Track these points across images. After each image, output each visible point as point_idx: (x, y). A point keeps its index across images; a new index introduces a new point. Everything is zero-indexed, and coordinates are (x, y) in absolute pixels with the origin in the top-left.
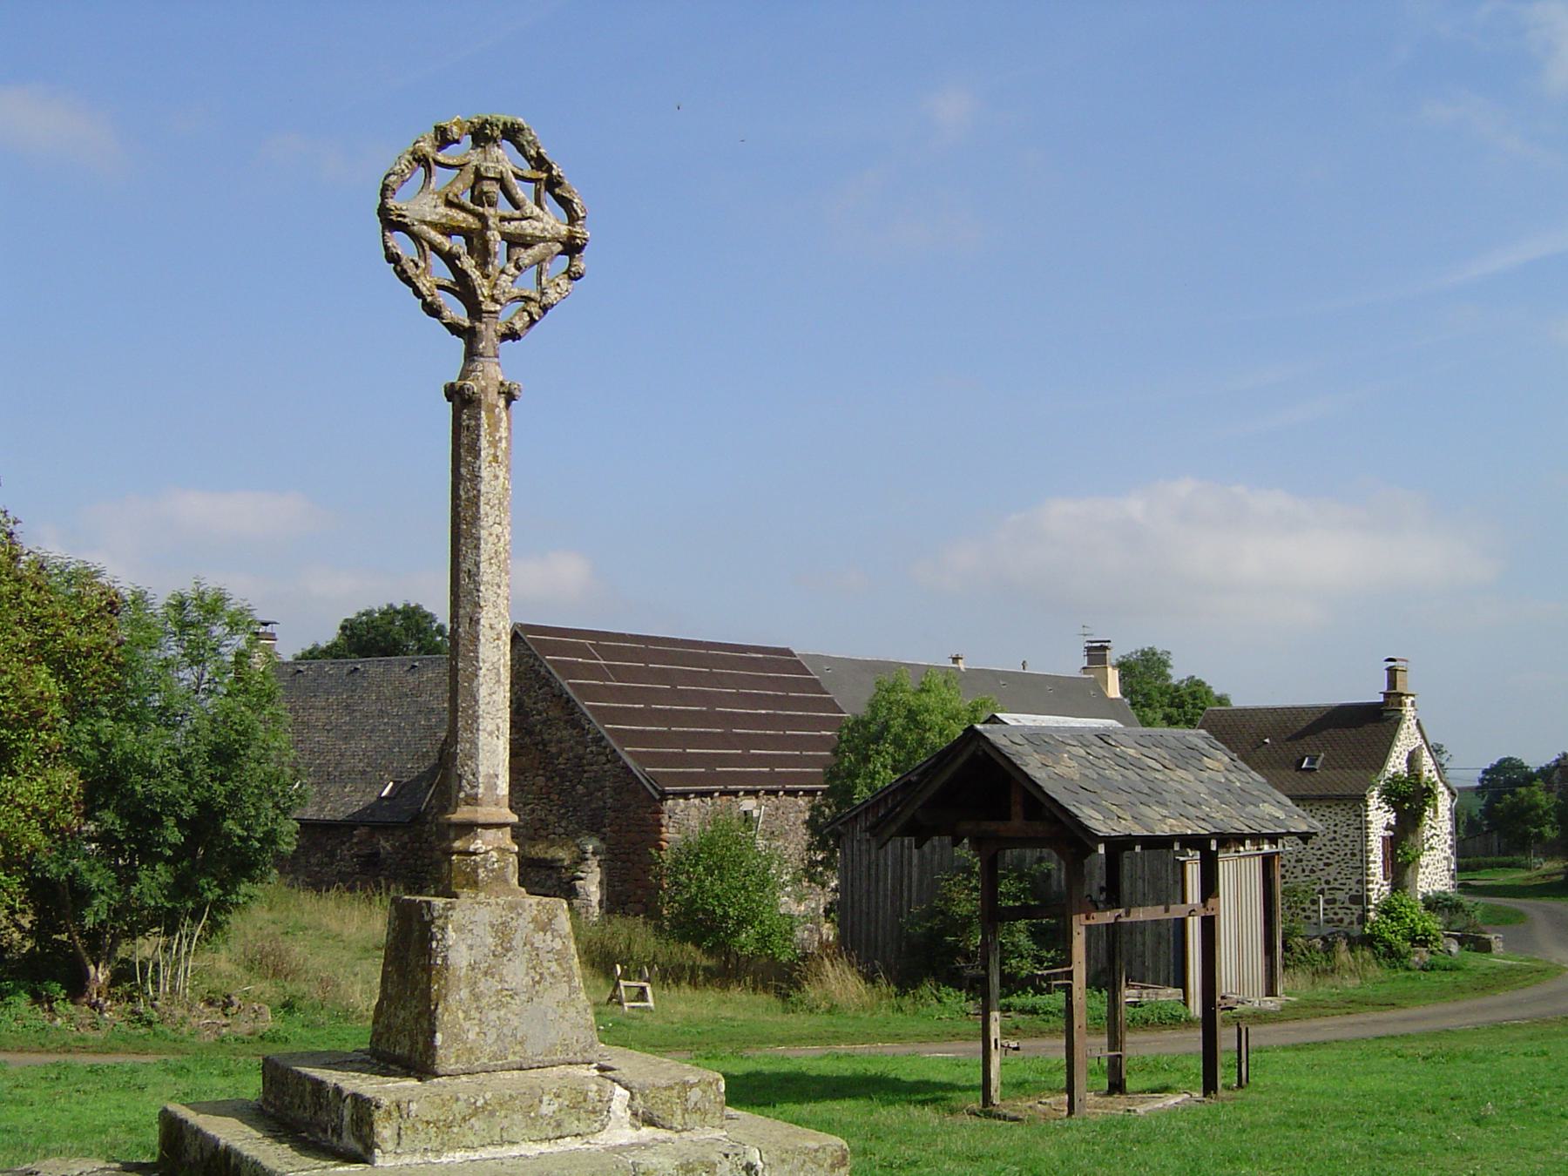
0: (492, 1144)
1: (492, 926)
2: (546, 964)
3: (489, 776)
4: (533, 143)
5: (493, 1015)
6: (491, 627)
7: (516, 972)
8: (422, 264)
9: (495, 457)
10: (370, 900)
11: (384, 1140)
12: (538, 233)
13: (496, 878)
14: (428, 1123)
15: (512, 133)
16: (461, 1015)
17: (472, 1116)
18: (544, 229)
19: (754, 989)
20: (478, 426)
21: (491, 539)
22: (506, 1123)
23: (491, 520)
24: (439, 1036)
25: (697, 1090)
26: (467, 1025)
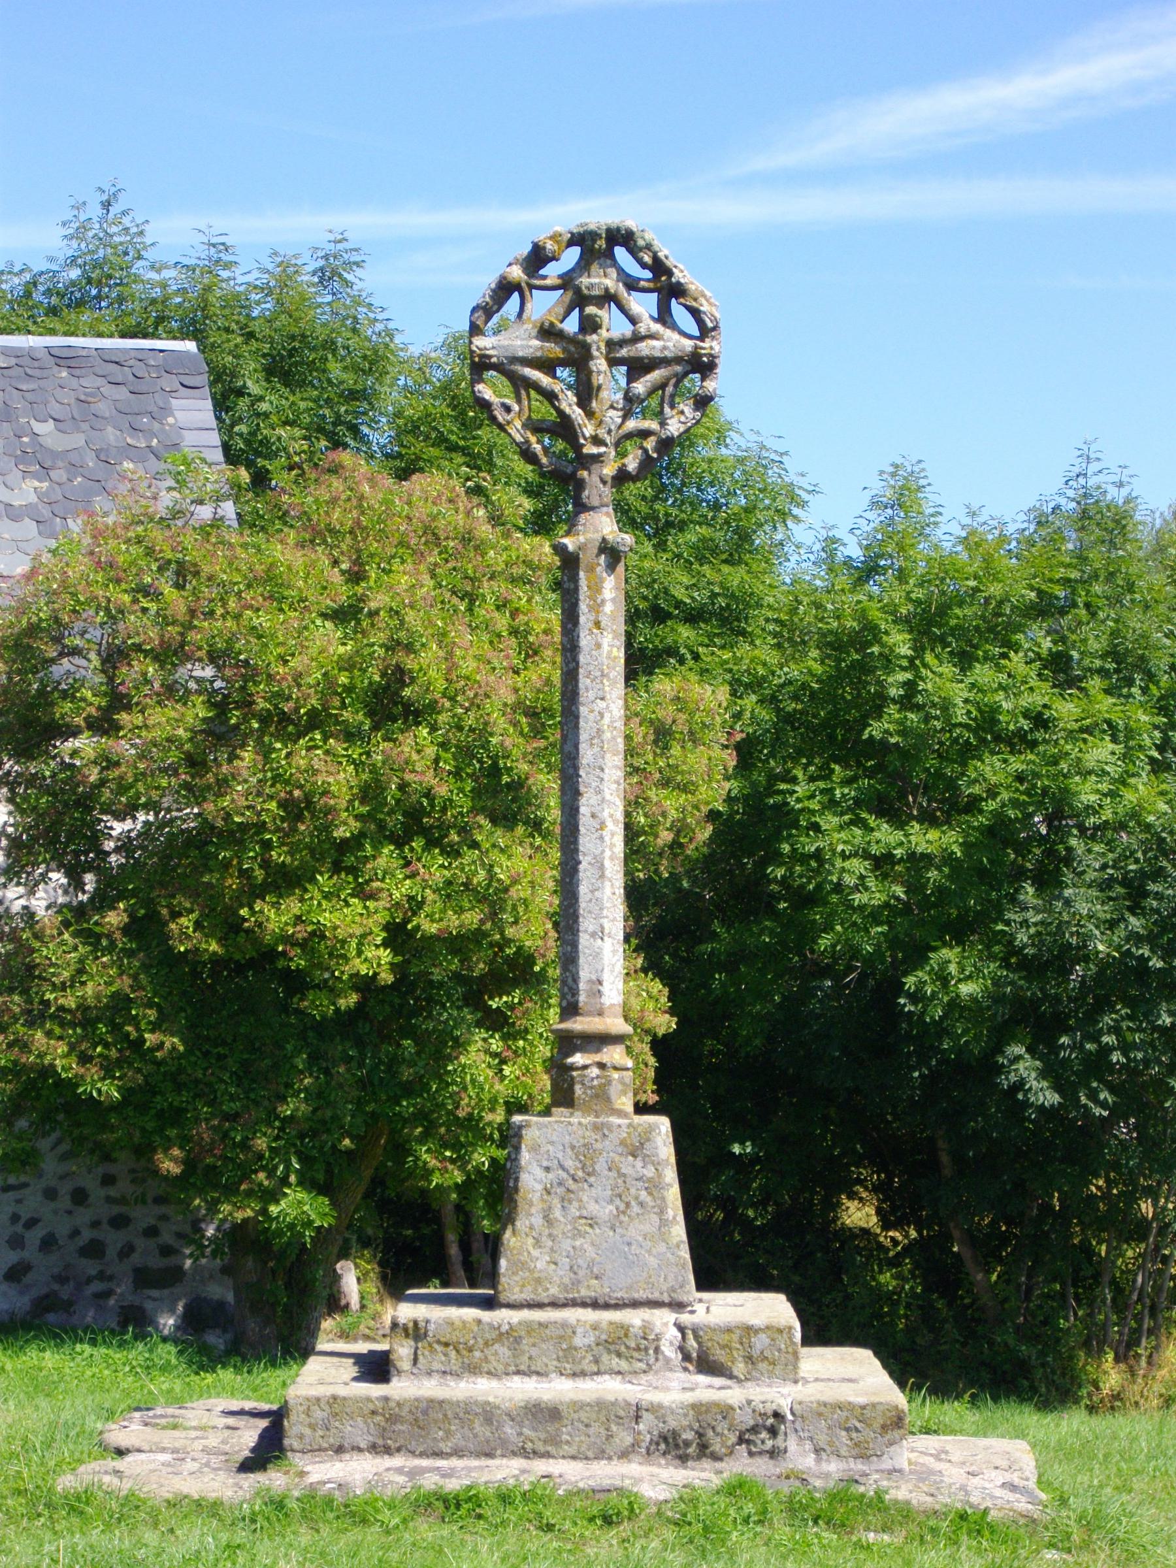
0: (518, 1373)
1: (573, 1147)
2: (633, 1191)
3: (590, 981)
4: (649, 247)
5: (566, 1245)
6: (593, 816)
7: (596, 1201)
8: (516, 408)
9: (597, 624)
10: (971, 541)
11: (401, 1358)
12: (657, 354)
13: (597, 1096)
14: (447, 1345)
15: (621, 237)
16: (530, 1241)
17: (495, 1341)
18: (665, 348)
19: (416, 1323)
20: (576, 590)
21: (591, 717)
22: (534, 1352)
23: (591, 695)
24: (503, 1263)
25: (762, 1336)
26: (535, 1253)
